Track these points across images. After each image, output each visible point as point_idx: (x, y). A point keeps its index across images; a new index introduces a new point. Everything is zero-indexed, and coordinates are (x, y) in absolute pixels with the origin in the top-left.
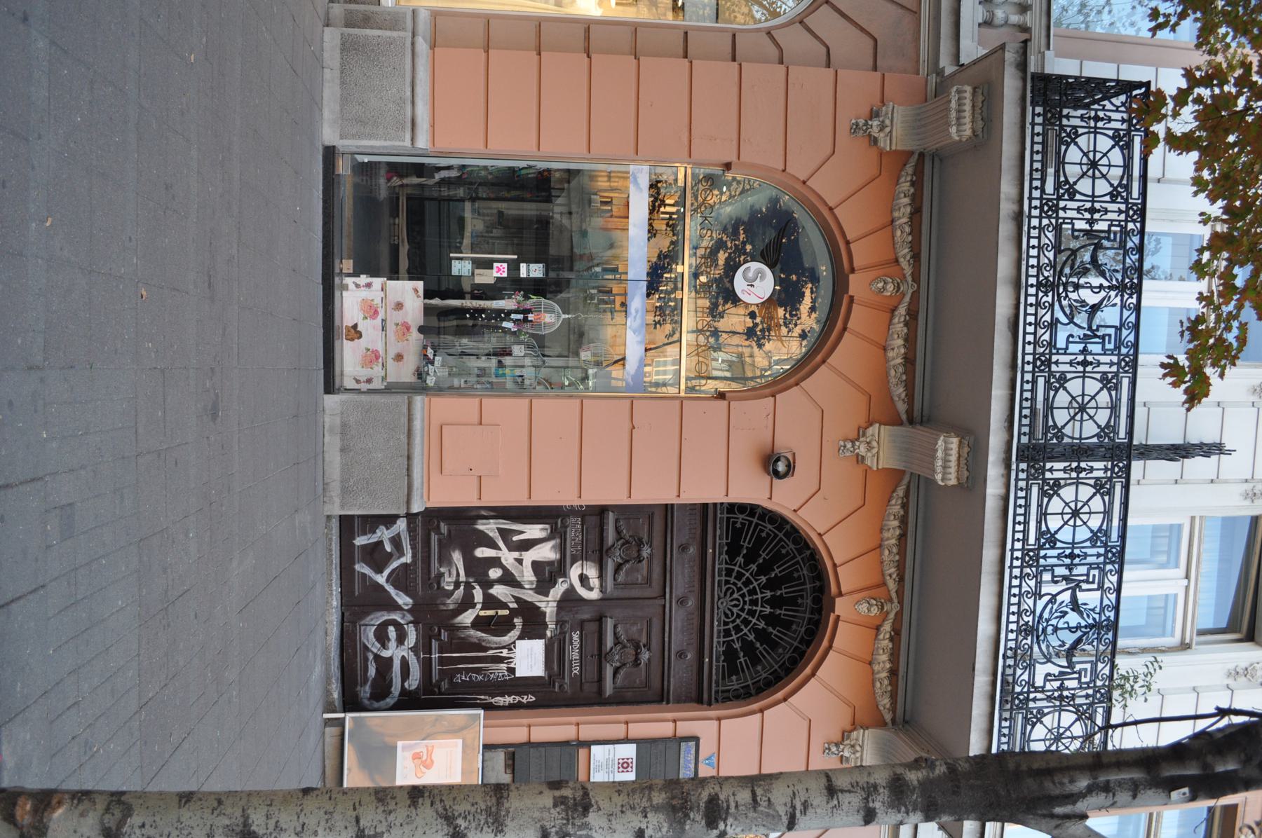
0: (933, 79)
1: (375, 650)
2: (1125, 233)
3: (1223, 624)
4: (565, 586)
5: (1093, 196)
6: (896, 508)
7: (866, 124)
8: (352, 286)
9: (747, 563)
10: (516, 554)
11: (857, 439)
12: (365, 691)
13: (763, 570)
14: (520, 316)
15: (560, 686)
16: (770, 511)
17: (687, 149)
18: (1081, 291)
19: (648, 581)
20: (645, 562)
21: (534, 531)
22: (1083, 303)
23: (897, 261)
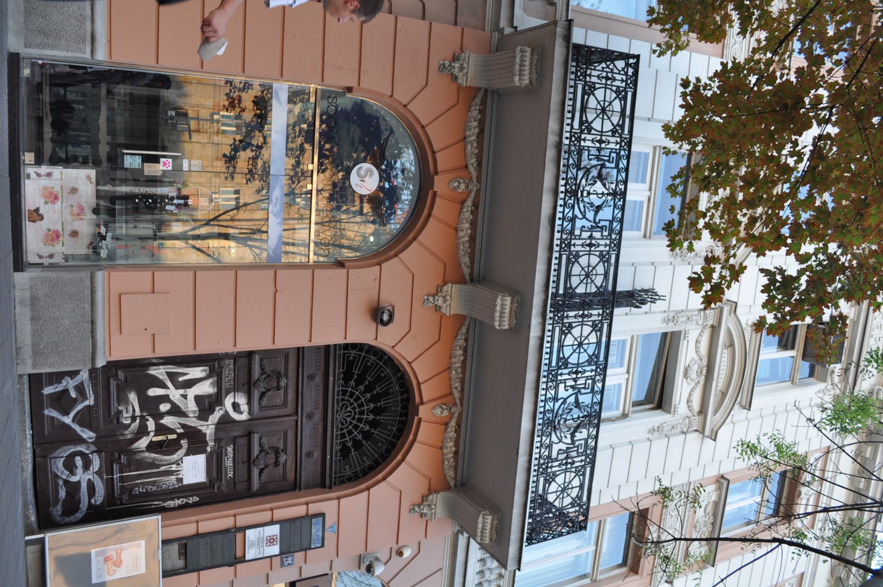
0: (496, 35)
1: (64, 477)
2: (619, 157)
3: (642, 398)
4: (222, 412)
5: (602, 132)
6: (461, 342)
7: (450, 65)
8: (33, 175)
9: (357, 385)
10: (182, 391)
11: (436, 294)
12: (57, 511)
13: (368, 389)
14: (181, 202)
15: (218, 488)
16: (374, 347)
17: (320, 75)
18: (591, 196)
19: (285, 404)
20: (282, 391)
21: (196, 372)
22: (592, 204)
23: (466, 167)
